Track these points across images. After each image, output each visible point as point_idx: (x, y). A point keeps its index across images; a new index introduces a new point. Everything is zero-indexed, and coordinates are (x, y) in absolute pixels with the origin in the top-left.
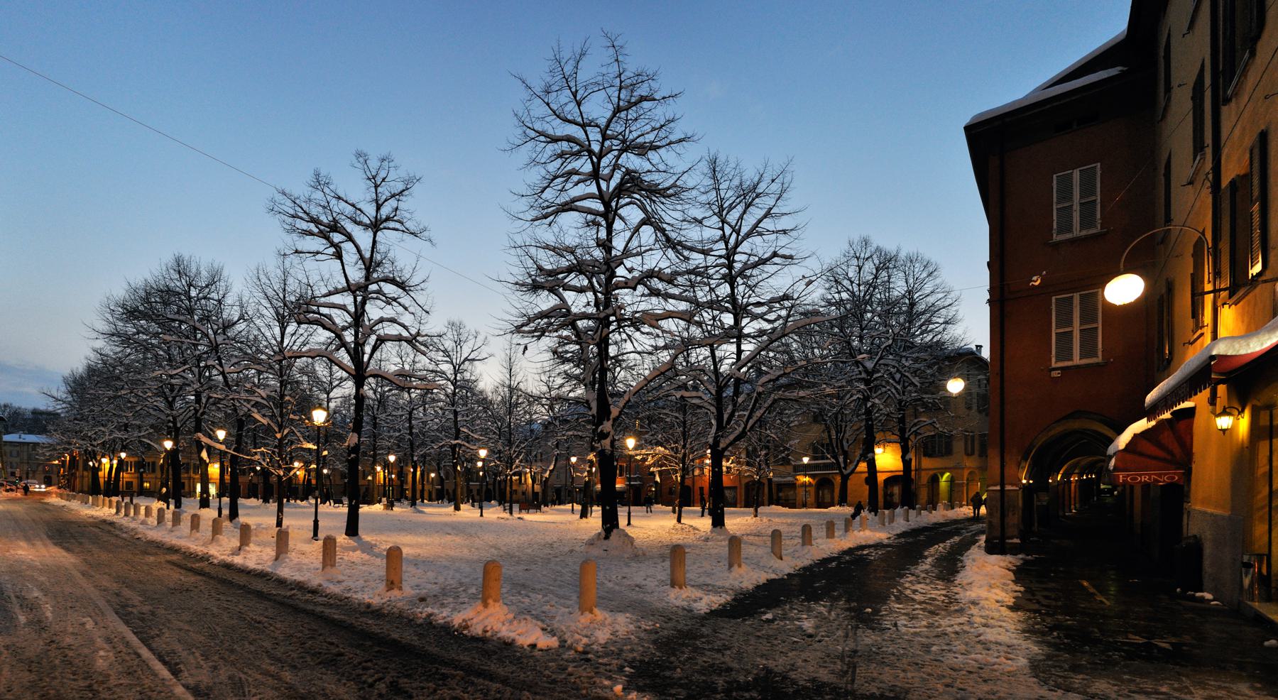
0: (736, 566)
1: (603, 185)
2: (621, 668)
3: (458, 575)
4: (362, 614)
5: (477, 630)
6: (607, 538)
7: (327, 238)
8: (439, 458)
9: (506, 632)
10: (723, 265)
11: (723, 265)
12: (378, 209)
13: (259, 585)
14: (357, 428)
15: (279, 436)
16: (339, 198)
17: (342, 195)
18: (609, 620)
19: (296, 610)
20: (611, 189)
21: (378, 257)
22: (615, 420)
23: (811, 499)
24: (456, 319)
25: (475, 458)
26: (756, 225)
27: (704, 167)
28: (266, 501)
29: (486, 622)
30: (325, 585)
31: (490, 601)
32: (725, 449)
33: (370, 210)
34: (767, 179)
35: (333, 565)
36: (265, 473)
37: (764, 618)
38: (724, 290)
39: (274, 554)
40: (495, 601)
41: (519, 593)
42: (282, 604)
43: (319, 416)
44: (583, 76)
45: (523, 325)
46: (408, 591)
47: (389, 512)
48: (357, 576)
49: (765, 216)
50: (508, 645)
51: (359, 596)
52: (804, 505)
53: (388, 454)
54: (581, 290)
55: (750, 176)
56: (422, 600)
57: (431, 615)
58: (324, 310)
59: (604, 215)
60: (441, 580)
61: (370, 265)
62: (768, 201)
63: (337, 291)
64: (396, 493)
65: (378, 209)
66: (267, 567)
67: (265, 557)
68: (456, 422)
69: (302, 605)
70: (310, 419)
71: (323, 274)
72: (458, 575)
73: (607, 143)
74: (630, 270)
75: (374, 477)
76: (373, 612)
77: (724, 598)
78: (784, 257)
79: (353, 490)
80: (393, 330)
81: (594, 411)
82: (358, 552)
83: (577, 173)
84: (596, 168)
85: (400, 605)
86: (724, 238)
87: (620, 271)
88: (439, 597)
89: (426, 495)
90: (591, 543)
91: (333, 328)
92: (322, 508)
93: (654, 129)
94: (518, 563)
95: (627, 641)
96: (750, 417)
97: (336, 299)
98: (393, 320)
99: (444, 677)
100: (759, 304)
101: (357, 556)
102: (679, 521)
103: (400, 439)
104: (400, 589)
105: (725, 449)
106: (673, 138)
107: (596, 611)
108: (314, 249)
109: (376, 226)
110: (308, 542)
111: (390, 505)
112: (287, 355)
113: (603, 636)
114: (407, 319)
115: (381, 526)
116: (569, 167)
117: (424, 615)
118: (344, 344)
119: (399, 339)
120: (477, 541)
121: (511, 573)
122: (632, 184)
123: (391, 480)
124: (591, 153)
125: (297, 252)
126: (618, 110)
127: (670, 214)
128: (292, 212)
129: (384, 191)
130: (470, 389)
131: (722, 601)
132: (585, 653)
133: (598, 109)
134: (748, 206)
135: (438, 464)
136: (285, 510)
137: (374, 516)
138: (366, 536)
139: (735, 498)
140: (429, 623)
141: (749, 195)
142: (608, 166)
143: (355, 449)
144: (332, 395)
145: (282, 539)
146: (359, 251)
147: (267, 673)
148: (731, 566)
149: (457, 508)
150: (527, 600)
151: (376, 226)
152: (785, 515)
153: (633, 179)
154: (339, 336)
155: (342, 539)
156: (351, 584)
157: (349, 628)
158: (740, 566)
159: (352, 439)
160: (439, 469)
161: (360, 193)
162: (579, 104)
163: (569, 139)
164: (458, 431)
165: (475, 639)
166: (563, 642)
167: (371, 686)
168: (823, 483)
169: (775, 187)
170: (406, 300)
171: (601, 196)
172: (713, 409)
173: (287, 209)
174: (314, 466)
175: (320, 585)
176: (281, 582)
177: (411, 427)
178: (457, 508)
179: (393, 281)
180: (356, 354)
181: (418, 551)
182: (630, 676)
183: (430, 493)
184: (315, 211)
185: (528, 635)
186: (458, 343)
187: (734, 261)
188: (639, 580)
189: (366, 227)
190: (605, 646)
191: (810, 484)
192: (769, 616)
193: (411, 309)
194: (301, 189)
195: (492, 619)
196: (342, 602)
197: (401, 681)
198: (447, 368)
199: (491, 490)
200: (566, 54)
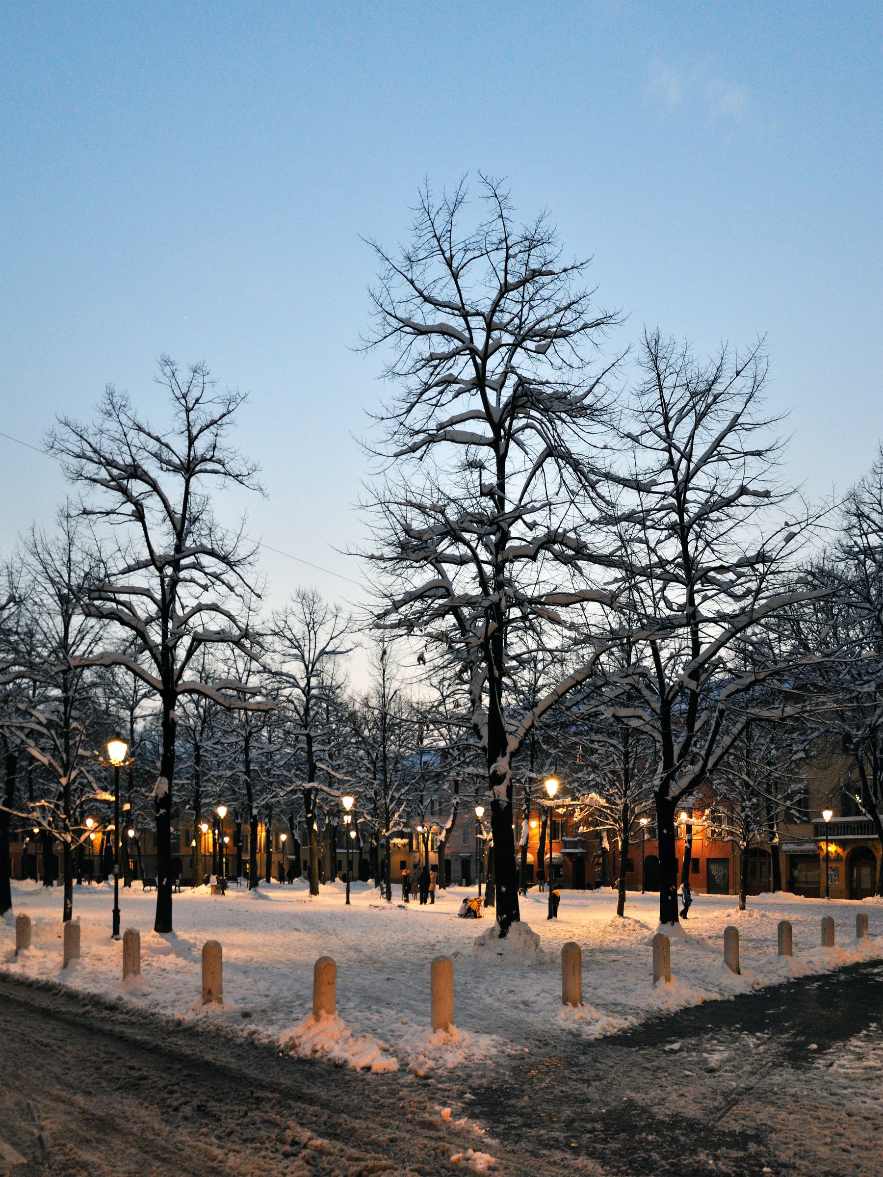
0: (662, 979)
1: (491, 395)
2: (461, 1095)
3: (297, 986)
4: (170, 1033)
5: (305, 1051)
6: (503, 935)
7: (124, 491)
8: (292, 810)
9: (338, 1052)
10: (669, 508)
11: (669, 508)
12: (192, 440)
13: (43, 1001)
14: (168, 771)
15: (64, 781)
16: (140, 429)
17: (144, 426)
18: (468, 1041)
19: (91, 1030)
20: (504, 400)
21: (194, 508)
22: (513, 755)
23: (839, 883)
24: (307, 587)
25: (339, 811)
26: (718, 443)
27: (641, 353)
28: (48, 883)
29: (317, 1040)
30: (126, 998)
31: (323, 1012)
32: (676, 799)
33: (180, 446)
34: (728, 373)
35: (137, 972)
36: (46, 838)
37: (668, 1047)
38: (671, 549)
39: (61, 959)
40: (329, 1012)
41: (369, 1008)
42: (73, 1024)
43: (117, 751)
44: (458, 236)
45: (386, 613)
46: (231, 1003)
47: (219, 898)
48: (168, 984)
49: (730, 429)
50: (339, 1067)
51: (168, 1012)
52: (828, 894)
53: (218, 804)
54: (461, 561)
55: (703, 365)
56: (246, 1015)
57: (254, 1033)
58: (123, 597)
59: (494, 444)
60: (274, 991)
61: (182, 523)
62: (736, 406)
63: (140, 565)
64: (236, 866)
65: (192, 440)
66: (54, 977)
67: (50, 965)
68: (310, 753)
69: (97, 1025)
70: (105, 753)
71: (119, 543)
72: (297, 986)
73: (496, 334)
74: (532, 526)
75: (199, 842)
76: (185, 1031)
77: (633, 1021)
78: (756, 494)
79: (168, 867)
80: (215, 623)
81: (485, 742)
82: (172, 956)
83: (455, 381)
84: (481, 371)
85: (219, 1021)
86: (671, 465)
87: (517, 529)
88: (265, 1014)
89: (274, 870)
90: (481, 943)
91: (134, 623)
92: (125, 894)
93: (558, 310)
94: (380, 970)
95: (481, 1066)
96: (709, 753)
97: (138, 579)
98: (214, 608)
99: (259, 1100)
100: (721, 569)
101: (170, 961)
102: (620, 912)
103: (234, 779)
104: (220, 1001)
105: (676, 799)
106: (588, 318)
107: (453, 1028)
108: (108, 507)
109: (188, 469)
110: (107, 943)
111: (221, 888)
112: (73, 663)
113: (453, 1059)
114: (233, 605)
115: (201, 917)
116: (444, 373)
117: (245, 1034)
118: (147, 645)
119: (221, 637)
120: (334, 939)
121: (367, 983)
122: (527, 397)
123: (222, 845)
124: (473, 352)
125: (85, 512)
126: (505, 289)
127: (579, 438)
128: (78, 451)
129: (199, 417)
130: (331, 701)
131: (625, 1024)
132: (427, 1077)
133: (479, 289)
134: (700, 417)
135: (291, 820)
136: (75, 896)
137: (195, 904)
138: (181, 932)
139: (725, 877)
140: (251, 1043)
141: (703, 398)
142: (497, 368)
143: (165, 801)
144: (138, 712)
145: (72, 933)
146: (167, 506)
147: (58, 1099)
148: (656, 979)
149: (314, 891)
150: (376, 1017)
151: (188, 469)
152: (809, 908)
153: (528, 393)
154: (142, 634)
155: (149, 937)
156: (160, 998)
157: (155, 1050)
158: (668, 979)
159: (161, 786)
160: (292, 827)
161: (168, 424)
162: (455, 276)
163: (445, 331)
164: (313, 768)
165: (302, 1061)
166: (404, 1068)
167: (176, 1109)
168: (858, 856)
169: (743, 384)
170: (230, 577)
171: (487, 415)
172: (658, 736)
173: (70, 447)
174: (112, 827)
175: (120, 999)
176: (72, 996)
177: (247, 763)
178: (314, 891)
179: (212, 553)
180: (165, 657)
181: (252, 954)
182: (471, 1104)
183: (281, 866)
184: (108, 448)
185: (365, 1055)
186: (311, 626)
187: (686, 501)
188: (529, 995)
189: (176, 469)
190: (452, 1071)
191: (838, 857)
192: (676, 1046)
193: (238, 590)
194: (89, 418)
195: (328, 1037)
196: (147, 1020)
197: (209, 1104)
198: (296, 668)
199: (368, 865)
200: (436, 202)
